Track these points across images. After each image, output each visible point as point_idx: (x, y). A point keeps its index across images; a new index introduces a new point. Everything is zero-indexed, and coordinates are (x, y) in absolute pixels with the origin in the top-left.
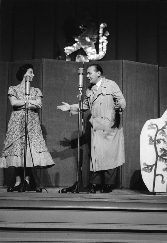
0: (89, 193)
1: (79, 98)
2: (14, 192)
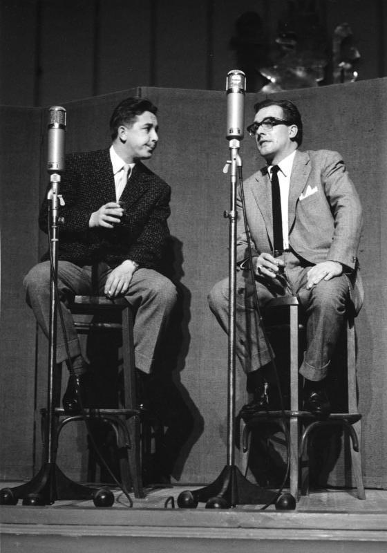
0: (273, 507)
1: (231, 176)
2: (115, 508)
